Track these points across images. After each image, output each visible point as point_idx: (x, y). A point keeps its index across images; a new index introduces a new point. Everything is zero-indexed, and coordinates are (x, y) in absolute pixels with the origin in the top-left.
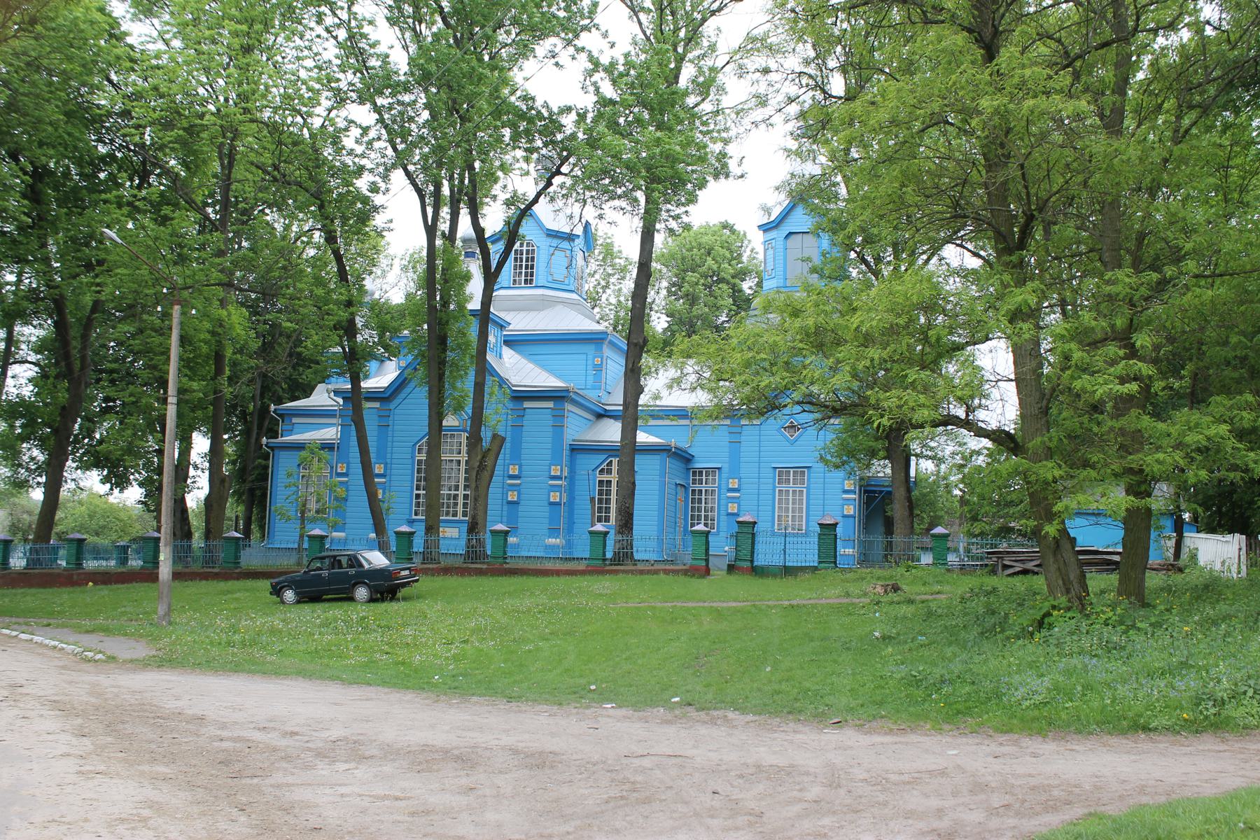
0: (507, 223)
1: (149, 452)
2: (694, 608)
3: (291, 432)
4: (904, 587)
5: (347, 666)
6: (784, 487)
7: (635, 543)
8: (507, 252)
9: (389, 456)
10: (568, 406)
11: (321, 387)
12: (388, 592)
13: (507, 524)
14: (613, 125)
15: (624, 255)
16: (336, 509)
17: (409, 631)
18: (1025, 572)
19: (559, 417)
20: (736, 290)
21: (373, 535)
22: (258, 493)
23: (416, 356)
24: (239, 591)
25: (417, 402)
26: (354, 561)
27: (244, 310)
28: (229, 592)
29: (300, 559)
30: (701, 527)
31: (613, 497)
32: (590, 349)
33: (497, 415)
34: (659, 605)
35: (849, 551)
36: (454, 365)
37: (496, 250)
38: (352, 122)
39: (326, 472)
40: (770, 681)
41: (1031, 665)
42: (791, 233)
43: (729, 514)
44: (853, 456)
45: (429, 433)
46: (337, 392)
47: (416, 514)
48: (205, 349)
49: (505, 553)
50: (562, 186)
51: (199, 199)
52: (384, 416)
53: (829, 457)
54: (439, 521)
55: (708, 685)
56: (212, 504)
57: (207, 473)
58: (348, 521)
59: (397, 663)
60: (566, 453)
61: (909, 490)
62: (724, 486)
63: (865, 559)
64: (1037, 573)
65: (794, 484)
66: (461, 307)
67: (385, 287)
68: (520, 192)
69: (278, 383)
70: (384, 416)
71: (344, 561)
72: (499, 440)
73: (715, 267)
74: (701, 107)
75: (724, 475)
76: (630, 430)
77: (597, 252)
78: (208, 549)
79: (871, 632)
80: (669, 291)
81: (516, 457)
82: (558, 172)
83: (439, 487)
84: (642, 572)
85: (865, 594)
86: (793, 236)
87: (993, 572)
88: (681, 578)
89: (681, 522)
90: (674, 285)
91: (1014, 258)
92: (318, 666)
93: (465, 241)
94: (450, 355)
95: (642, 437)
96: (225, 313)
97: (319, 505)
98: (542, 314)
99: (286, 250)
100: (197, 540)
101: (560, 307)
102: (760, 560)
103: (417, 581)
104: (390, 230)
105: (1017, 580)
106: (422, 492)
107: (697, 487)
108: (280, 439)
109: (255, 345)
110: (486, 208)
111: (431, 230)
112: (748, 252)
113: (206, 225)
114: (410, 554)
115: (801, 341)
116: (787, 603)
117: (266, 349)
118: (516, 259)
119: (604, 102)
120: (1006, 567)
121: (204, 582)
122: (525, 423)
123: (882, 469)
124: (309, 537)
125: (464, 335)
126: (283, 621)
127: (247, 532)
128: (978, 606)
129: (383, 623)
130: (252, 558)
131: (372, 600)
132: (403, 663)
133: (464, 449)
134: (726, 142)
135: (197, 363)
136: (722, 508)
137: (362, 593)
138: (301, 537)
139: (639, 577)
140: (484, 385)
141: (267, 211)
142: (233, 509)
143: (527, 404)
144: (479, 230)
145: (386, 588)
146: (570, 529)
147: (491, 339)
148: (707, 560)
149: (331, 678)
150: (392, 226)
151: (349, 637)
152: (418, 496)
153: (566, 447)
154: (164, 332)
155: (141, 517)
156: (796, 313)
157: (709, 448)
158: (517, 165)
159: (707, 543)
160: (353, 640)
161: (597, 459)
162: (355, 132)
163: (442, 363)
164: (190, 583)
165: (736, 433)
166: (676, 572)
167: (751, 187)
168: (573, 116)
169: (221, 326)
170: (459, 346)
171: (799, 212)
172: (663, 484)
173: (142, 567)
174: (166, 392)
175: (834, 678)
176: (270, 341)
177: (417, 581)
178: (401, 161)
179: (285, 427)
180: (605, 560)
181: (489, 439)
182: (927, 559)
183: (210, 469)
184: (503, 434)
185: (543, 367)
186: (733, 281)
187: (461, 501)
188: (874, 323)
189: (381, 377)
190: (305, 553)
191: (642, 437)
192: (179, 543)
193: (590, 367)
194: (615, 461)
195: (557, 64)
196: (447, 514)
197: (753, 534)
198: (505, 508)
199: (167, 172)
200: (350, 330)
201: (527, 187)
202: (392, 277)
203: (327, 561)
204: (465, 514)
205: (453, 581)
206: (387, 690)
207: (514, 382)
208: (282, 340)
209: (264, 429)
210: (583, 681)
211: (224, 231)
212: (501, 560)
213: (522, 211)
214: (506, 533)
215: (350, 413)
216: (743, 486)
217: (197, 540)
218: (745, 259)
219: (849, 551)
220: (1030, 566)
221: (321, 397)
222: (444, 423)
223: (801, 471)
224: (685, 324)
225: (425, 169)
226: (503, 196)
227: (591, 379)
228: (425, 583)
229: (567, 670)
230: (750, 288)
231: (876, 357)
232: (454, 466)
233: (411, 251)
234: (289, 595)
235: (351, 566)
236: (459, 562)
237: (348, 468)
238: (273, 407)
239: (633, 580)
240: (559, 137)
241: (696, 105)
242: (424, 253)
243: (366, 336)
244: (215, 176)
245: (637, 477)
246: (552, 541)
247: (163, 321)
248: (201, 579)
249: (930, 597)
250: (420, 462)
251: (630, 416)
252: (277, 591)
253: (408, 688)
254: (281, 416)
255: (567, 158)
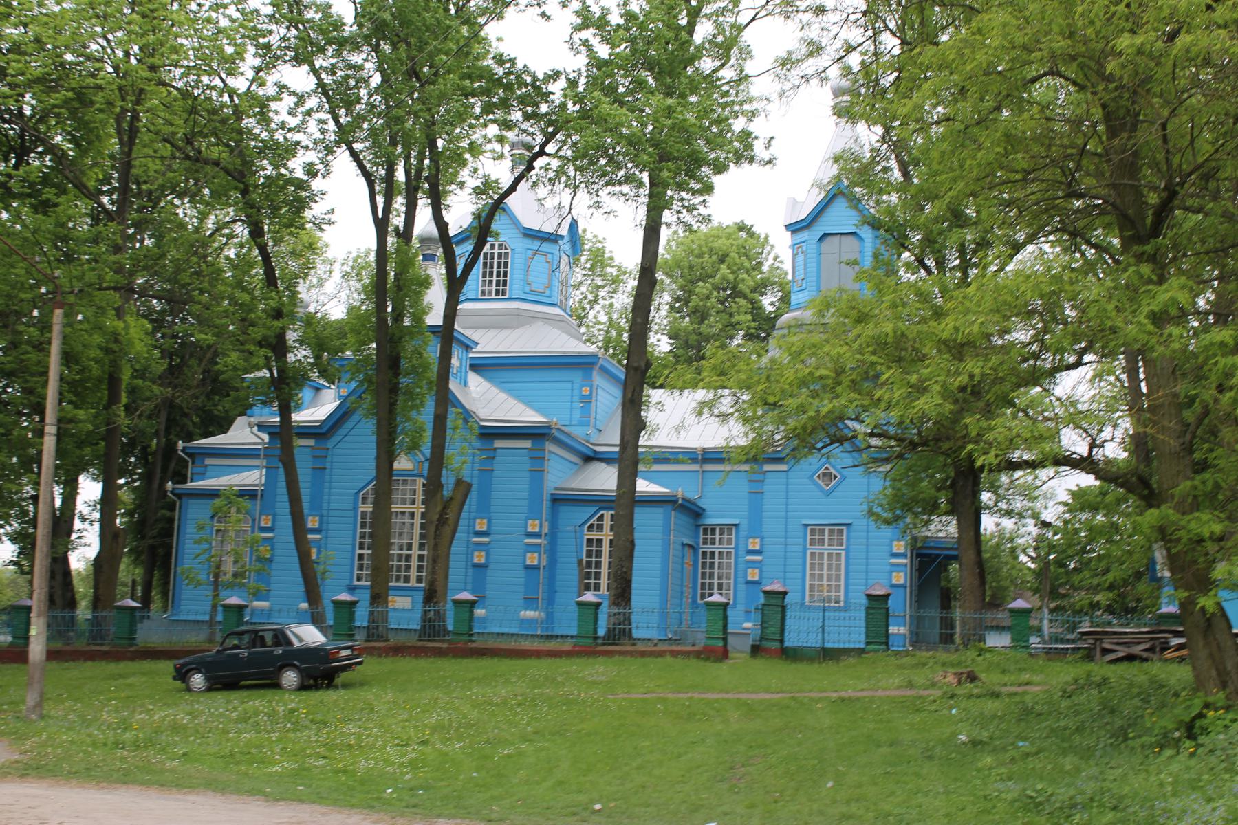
0: (477, 216)
1: (24, 500)
2: (717, 701)
3: (203, 476)
4: (983, 676)
5: (270, 775)
6: (817, 549)
7: (633, 618)
8: (474, 253)
9: (325, 506)
10: (550, 447)
11: (240, 421)
12: (324, 678)
13: (473, 592)
14: (611, 91)
15: (616, 263)
16: (258, 572)
17: (351, 729)
18: (1130, 658)
19: (538, 459)
20: (756, 308)
21: (305, 605)
22: (161, 551)
23: (361, 383)
24: (134, 674)
25: (362, 437)
26: (281, 638)
27: (146, 322)
28: (121, 676)
29: (213, 634)
30: (716, 598)
31: (605, 560)
32: (577, 376)
33: (461, 456)
34: (670, 696)
35: (903, 630)
36: (410, 393)
37: (463, 251)
38: (284, 87)
39: (246, 526)
40: (835, 802)
41: (1194, 785)
42: (826, 235)
43: (748, 583)
44: (909, 510)
45: (377, 478)
46: (262, 427)
47: (359, 579)
48: (96, 370)
49: (471, 628)
50: (547, 168)
51: (91, 184)
52: (320, 457)
53: (879, 510)
54: (388, 588)
55: (752, 806)
56: (103, 565)
57: (97, 526)
58: (273, 587)
59: (337, 772)
60: (546, 504)
61: (979, 552)
62: (741, 547)
63: (917, 640)
64: (1146, 660)
65: (834, 542)
66: (418, 319)
67: (321, 298)
68: (493, 178)
69: (186, 415)
70: (320, 457)
71: (268, 637)
72: (463, 488)
73: (731, 277)
74: (721, 73)
75: (742, 534)
76: (628, 477)
77: (583, 259)
78: (96, 621)
79: (954, 735)
80: (672, 308)
81: (484, 509)
82: (542, 153)
83: (389, 546)
84: (643, 654)
85: (933, 685)
86: (829, 239)
87: (1089, 656)
88: (693, 662)
89: (688, 592)
90: (678, 300)
91: (1148, 248)
92: (232, 776)
93: (424, 240)
94: (404, 381)
95: (643, 486)
96: (121, 324)
97: (237, 568)
98: (518, 332)
99: (199, 246)
100: (83, 611)
101: (540, 323)
102: (791, 641)
103: (360, 663)
104: (330, 223)
105: (1122, 667)
106: (366, 552)
107: (709, 548)
108: (190, 485)
109: (160, 367)
110: (449, 198)
111: (381, 225)
112: (771, 261)
113: (99, 215)
114: (351, 628)
115: (874, 353)
116: (835, 695)
117: (173, 374)
118: (485, 264)
119: (597, 63)
120: (1105, 651)
121: (89, 663)
122: (495, 467)
123: (945, 528)
124: (225, 606)
125: (421, 354)
126: (189, 714)
127: (146, 601)
128: (1090, 699)
129: (318, 718)
130: (150, 633)
131: (303, 687)
132: (345, 772)
133: (420, 497)
134: (754, 114)
135: (86, 388)
136: (740, 574)
137: (290, 678)
138: (214, 607)
139: (640, 660)
140: (446, 418)
141: (177, 202)
142: (128, 571)
143: (498, 444)
144: (442, 225)
145: (320, 672)
146: (550, 601)
147: (455, 361)
148: (725, 640)
149: (252, 792)
150: (333, 218)
151: (274, 736)
152: (361, 557)
153: (546, 497)
154: (42, 347)
155: (13, 581)
156: (862, 319)
157: (723, 500)
158: (489, 147)
159: (725, 618)
160: (279, 740)
161: (585, 512)
162: (289, 101)
163: (394, 390)
164: (71, 664)
165: (757, 482)
166: (687, 654)
167: (787, 163)
168: (562, 83)
169: (117, 341)
170: (414, 370)
171: (840, 206)
172: (667, 544)
173: (11, 643)
174: (42, 420)
175: (920, 799)
176: (179, 357)
177: (360, 663)
178: (345, 136)
179: (197, 470)
180: (596, 638)
181: (451, 486)
182: (998, 641)
183: (102, 521)
184: (468, 479)
185: (518, 397)
186: (751, 295)
187: (414, 563)
188: (976, 328)
189: (317, 408)
190: (218, 627)
191: (643, 486)
192: (59, 613)
193: (576, 398)
194: (607, 515)
195: (543, 14)
196: (398, 579)
197: (784, 608)
198: (470, 571)
199: (52, 150)
200: (279, 347)
201: (503, 173)
202: (330, 287)
203: (246, 638)
204: (419, 580)
205: (405, 664)
206: (324, 809)
207: (482, 417)
208: (193, 362)
209: (170, 473)
210: (583, 798)
211: (122, 221)
212: (465, 638)
213: (494, 205)
214: (472, 604)
215: (278, 452)
216: (766, 548)
217: (83, 611)
218: (765, 268)
219: (903, 630)
220: (1137, 650)
221: (242, 433)
222: (396, 466)
223: (838, 529)
224: (691, 350)
225: (376, 144)
226: (472, 183)
227: (577, 414)
228: (370, 666)
229: (561, 783)
230: (772, 304)
231: (977, 371)
232: (407, 520)
233: (354, 254)
234: (197, 680)
235: (277, 643)
236: (412, 640)
237: (274, 521)
238: (180, 444)
239: (634, 664)
240: (544, 108)
241: (715, 71)
242: (372, 257)
243: (299, 355)
244: (112, 157)
245: (636, 535)
246: (530, 614)
247: (42, 335)
248: (86, 660)
249: (1020, 690)
250: (364, 514)
251: (629, 459)
252: (182, 675)
253: (352, 806)
254: (191, 455)
255: (553, 135)
